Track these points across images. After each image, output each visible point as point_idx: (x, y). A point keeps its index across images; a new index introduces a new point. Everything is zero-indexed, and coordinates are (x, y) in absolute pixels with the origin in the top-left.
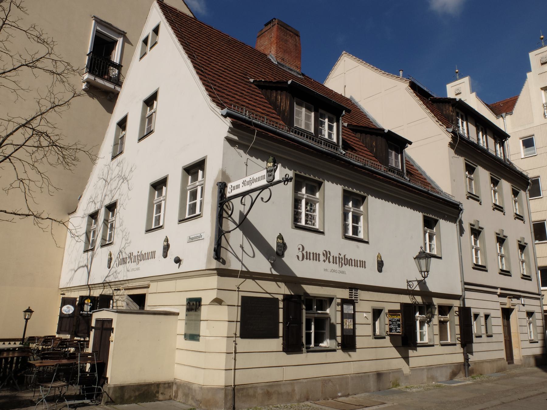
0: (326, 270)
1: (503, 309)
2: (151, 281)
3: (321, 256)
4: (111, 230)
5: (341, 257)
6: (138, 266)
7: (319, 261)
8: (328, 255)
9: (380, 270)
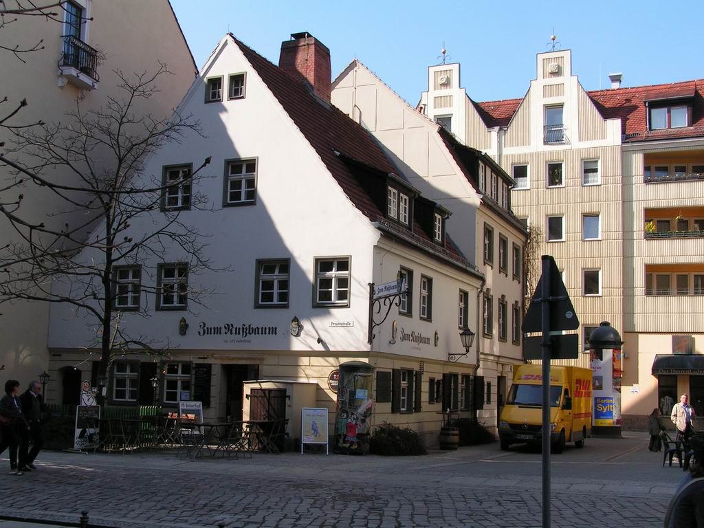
1: (498, 377)
4: (424, 308)
6: (246, 339)
7: (220, 333)
8: (231, 328)
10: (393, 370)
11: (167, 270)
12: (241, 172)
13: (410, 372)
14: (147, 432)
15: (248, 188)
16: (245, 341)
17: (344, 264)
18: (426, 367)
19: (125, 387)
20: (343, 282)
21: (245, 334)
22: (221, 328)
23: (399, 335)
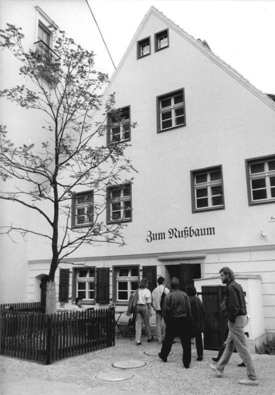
5: (186, 229)
11: (113, 191)
15: (177, 116)
17: (216, 172)
19: (85, 289)
20: (218, 190)
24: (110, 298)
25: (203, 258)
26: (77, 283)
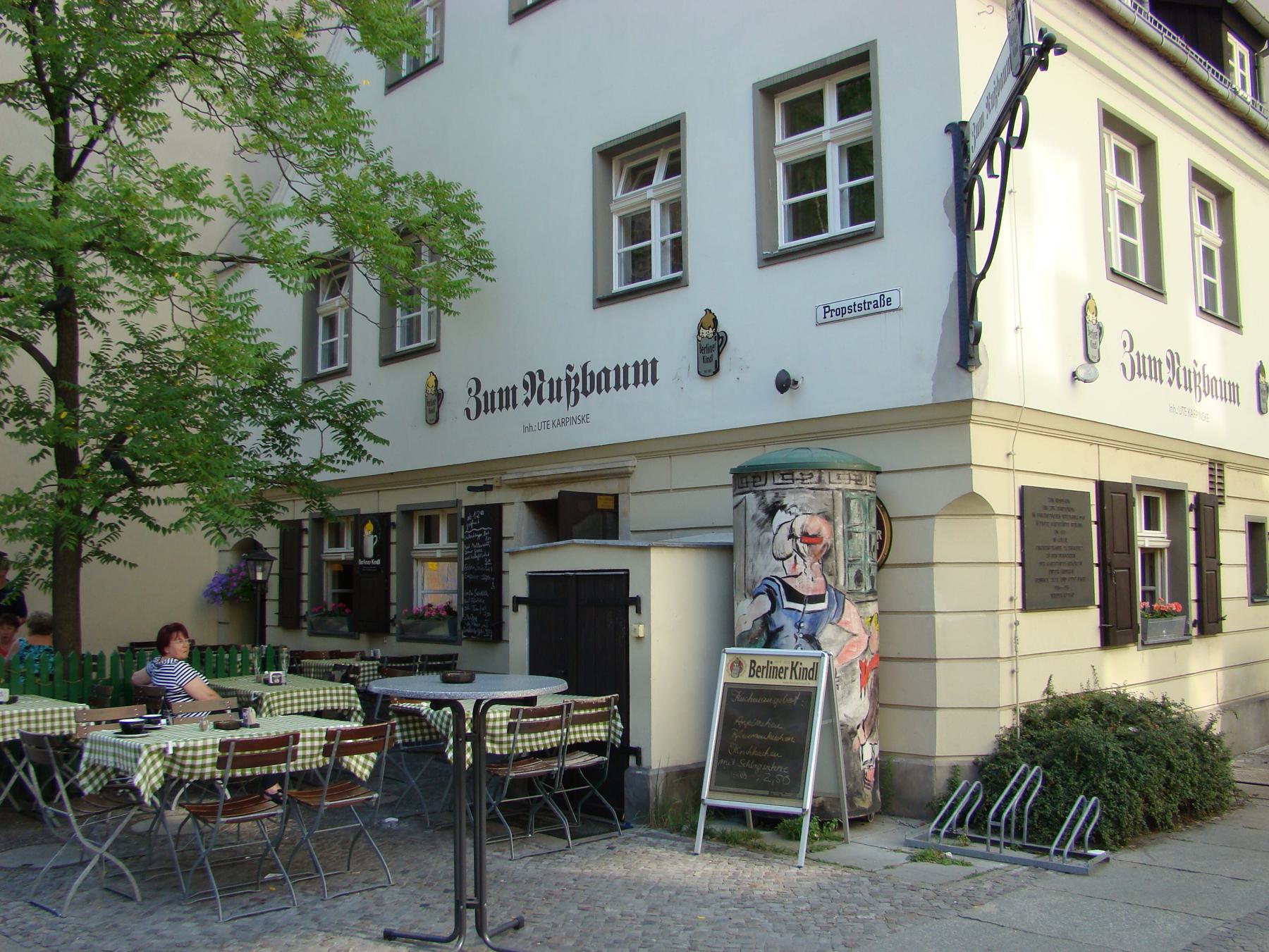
0: (1172, 408)
2: (641, 456)
3: (1164, 365)
5: (572, 374)
6: (575, 412)
8: (538, 382)
9: (135, 565)
10: (1100, 485)
12: (820, 123)
13: (1174, 495)
14: (153, 763)
16: (574, 420)
18: (1233, 482)
21: (572, 394)
22: (514, 388)
23: (1111, 350)
24: (304, 613)
25: (624, 474)
26: (1097, 602)
